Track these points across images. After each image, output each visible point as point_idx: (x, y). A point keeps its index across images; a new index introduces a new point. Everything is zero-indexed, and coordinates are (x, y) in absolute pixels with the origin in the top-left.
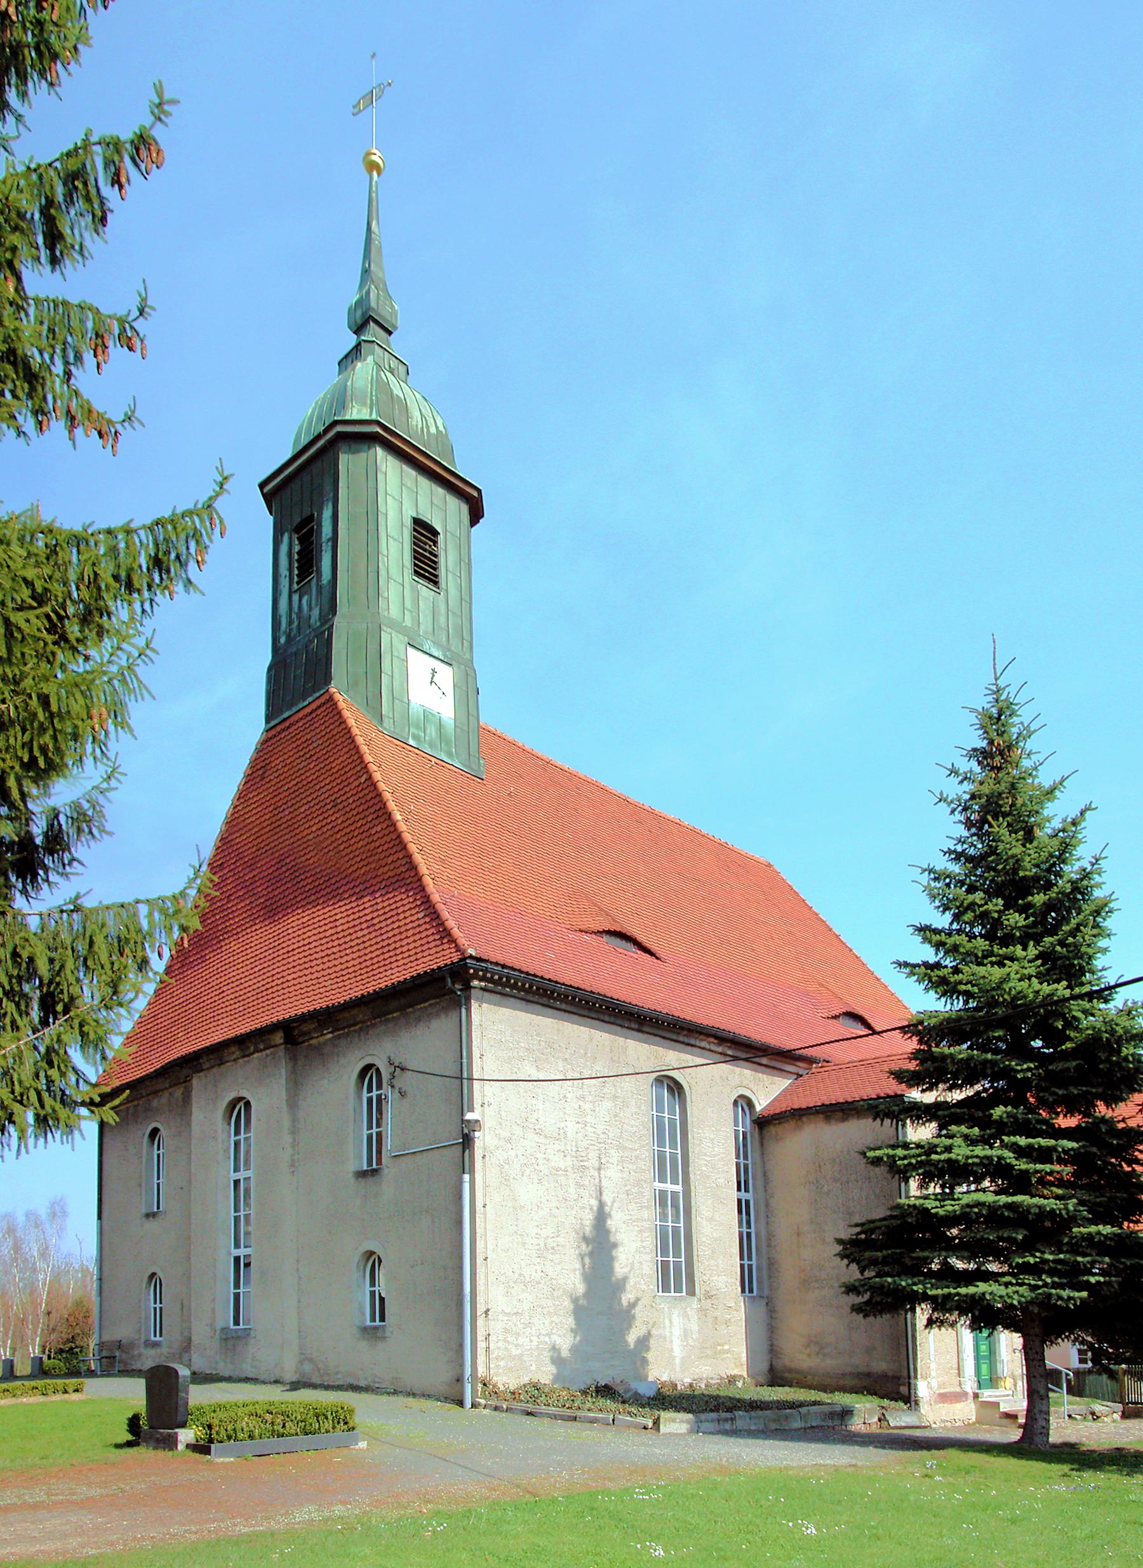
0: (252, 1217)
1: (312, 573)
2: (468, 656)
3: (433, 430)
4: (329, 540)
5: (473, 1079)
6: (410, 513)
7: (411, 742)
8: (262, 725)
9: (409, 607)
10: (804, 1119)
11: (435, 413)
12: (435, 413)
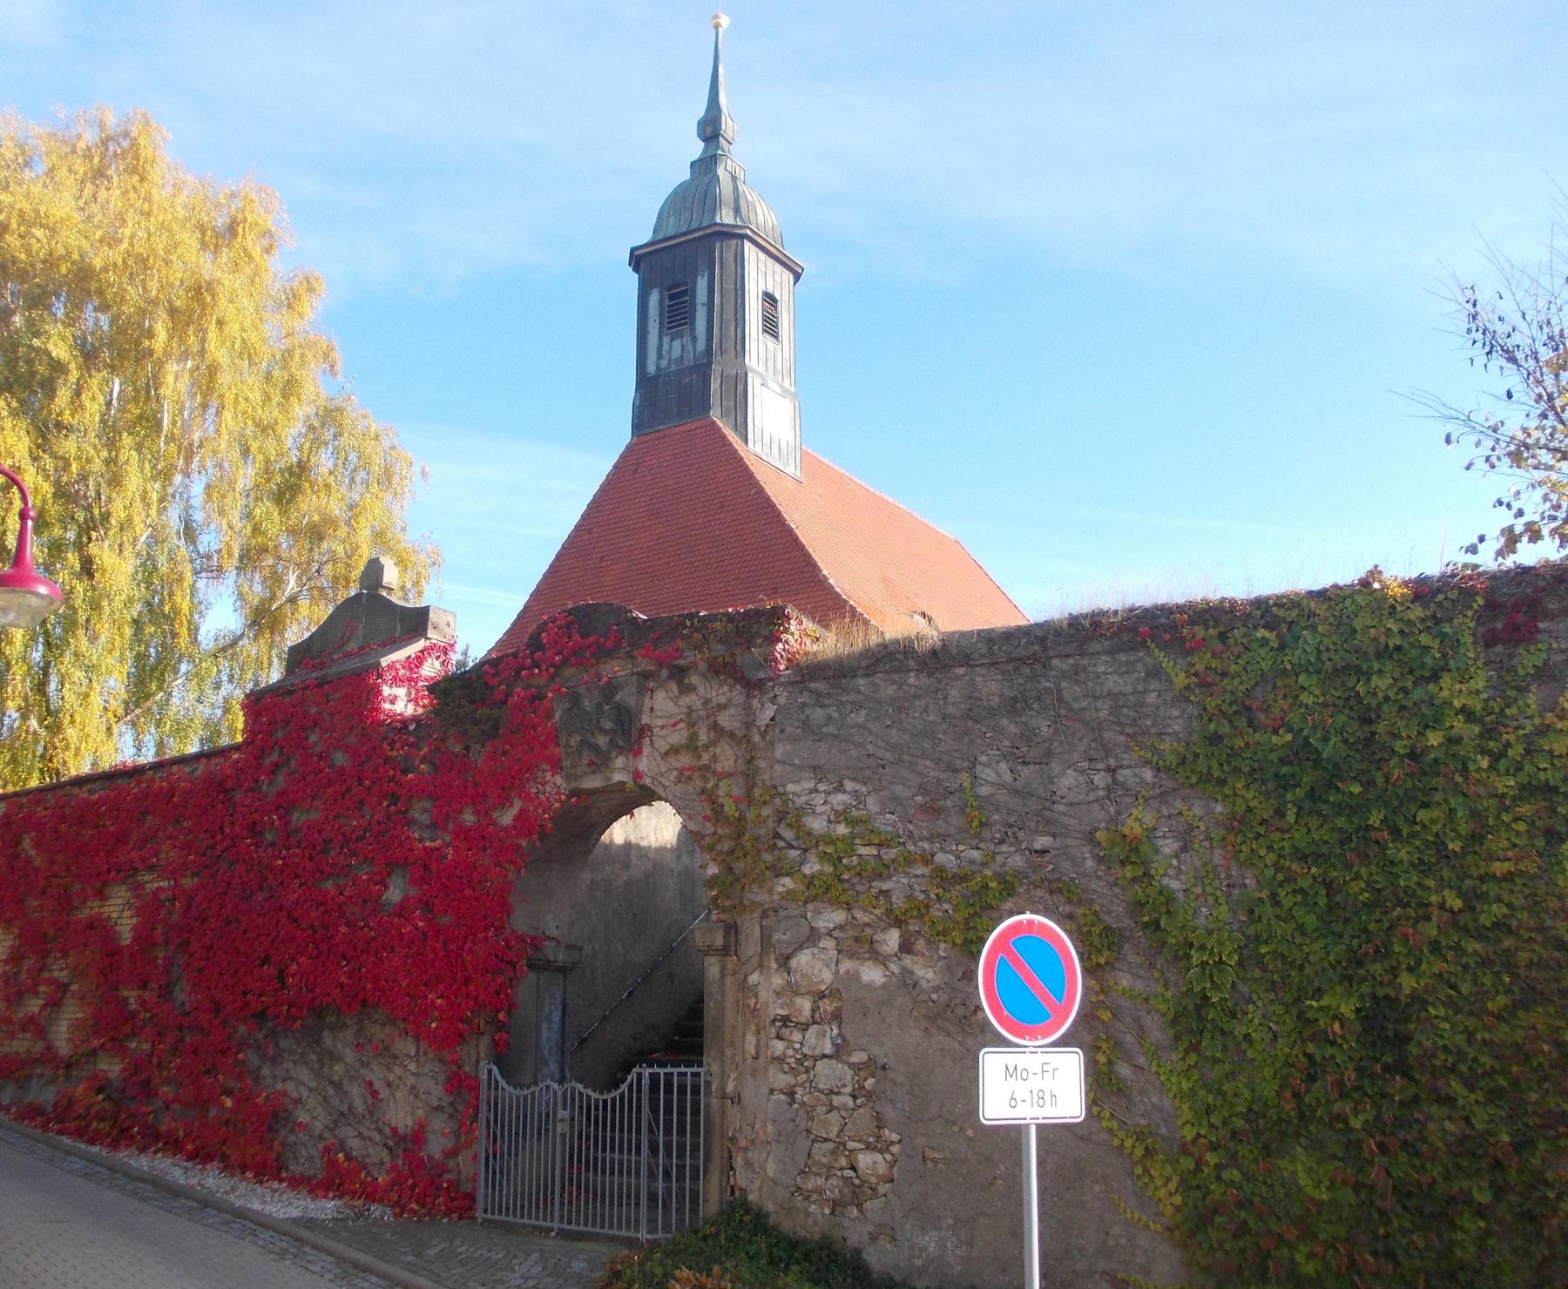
6: (762, 288)
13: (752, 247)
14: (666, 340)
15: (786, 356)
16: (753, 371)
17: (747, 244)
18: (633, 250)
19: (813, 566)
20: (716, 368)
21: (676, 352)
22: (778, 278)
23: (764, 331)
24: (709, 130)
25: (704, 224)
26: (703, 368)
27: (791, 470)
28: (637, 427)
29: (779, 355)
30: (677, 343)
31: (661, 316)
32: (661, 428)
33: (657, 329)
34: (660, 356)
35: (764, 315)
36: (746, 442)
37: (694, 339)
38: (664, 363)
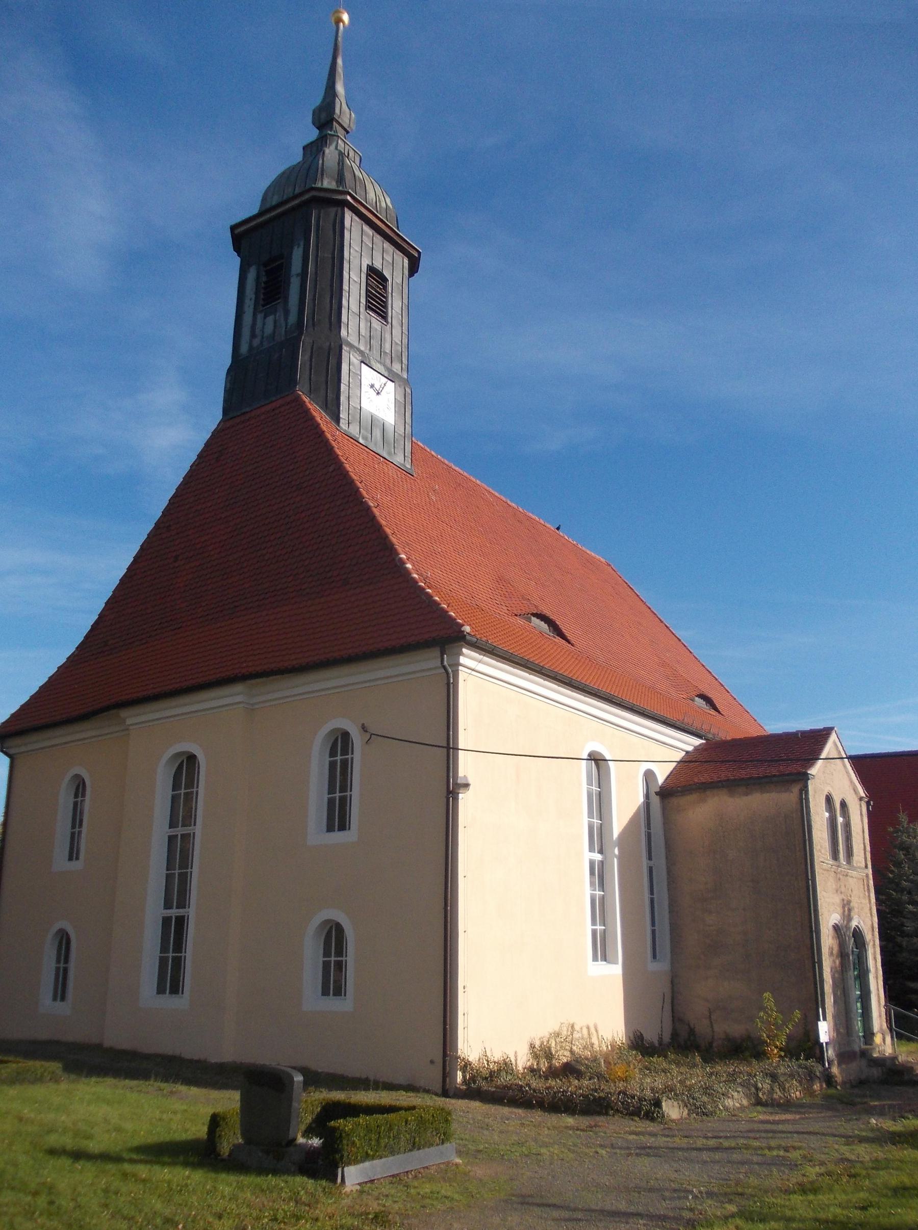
0: (655, 899)
1: (279, 298)
2: (359, 373)
3: (384, 205)
4: (298, 275)
5: (459, 749)
6: (366, 262)
7: (361, 441)
8: (218, 415)
9: (363, 334)
10: (708, 793)
11: (384, 193)
12: (384, 193)
13: (356, 218)
14: (260, 317)
15: (397, 339)
16: (351, 346)
17: (348, 215)
18: (233, 228)
19: (391, 550)
20: (305, 341)
21: (269, 329)
22: (389, 258)
23: (368, 307)
24: (323, 116)
25: (297, 191)
26: (292, 344)
27: (398, 459)
28: (225, 411)
29: (388, 336)
30: (270, 319)
31: (257, 293)
32: (248, 409)
33: (252, 307)
34: (253, 335)
35: (367, 290)
36: (337, 420)
37: (287, 312)
38: (256, 342)
